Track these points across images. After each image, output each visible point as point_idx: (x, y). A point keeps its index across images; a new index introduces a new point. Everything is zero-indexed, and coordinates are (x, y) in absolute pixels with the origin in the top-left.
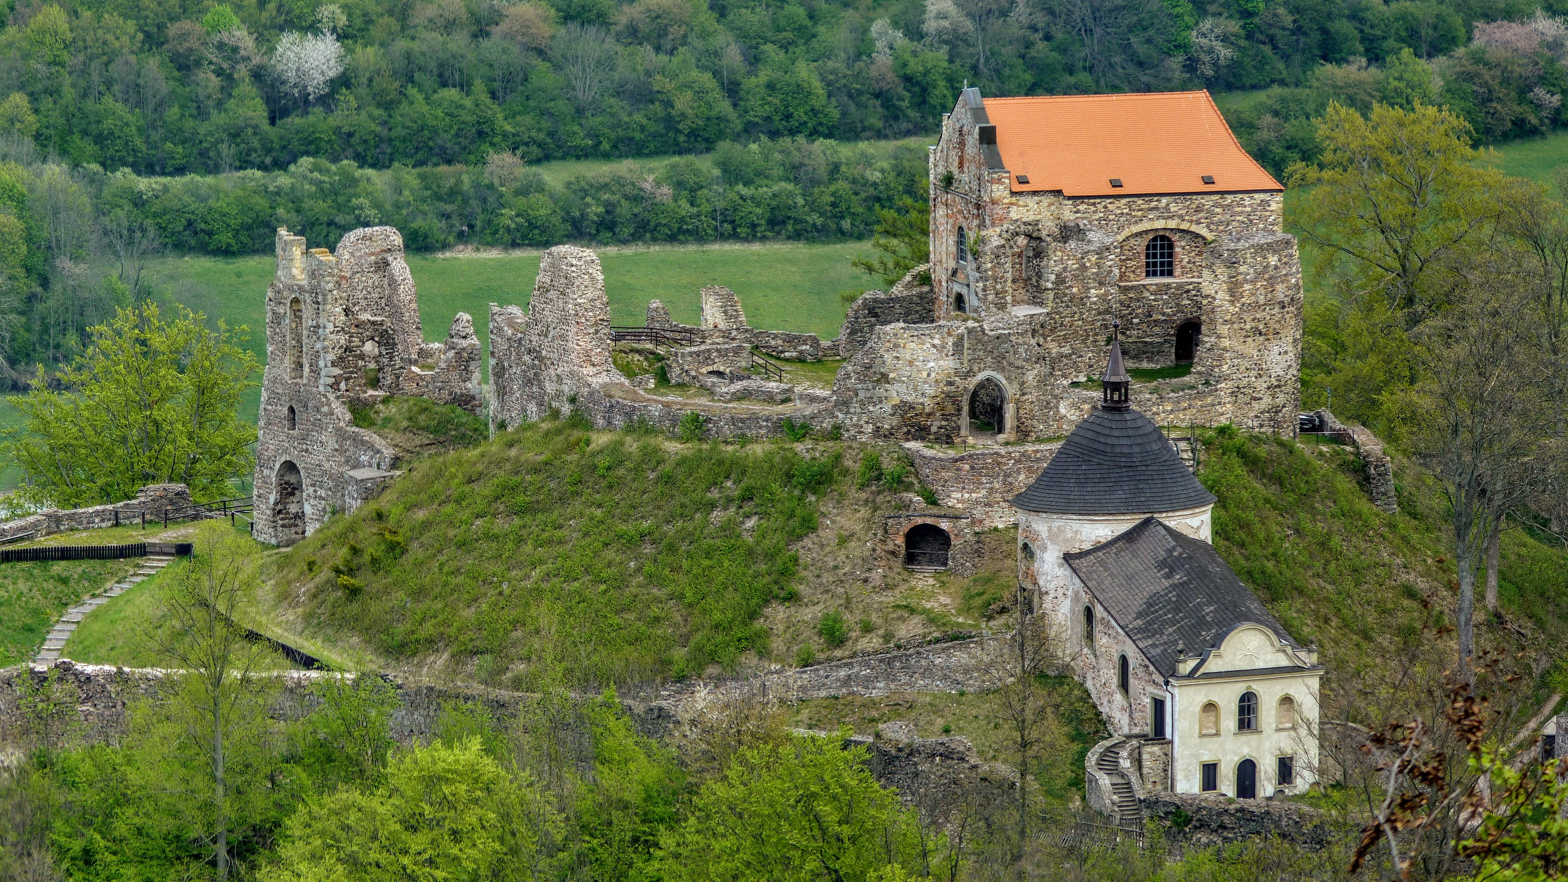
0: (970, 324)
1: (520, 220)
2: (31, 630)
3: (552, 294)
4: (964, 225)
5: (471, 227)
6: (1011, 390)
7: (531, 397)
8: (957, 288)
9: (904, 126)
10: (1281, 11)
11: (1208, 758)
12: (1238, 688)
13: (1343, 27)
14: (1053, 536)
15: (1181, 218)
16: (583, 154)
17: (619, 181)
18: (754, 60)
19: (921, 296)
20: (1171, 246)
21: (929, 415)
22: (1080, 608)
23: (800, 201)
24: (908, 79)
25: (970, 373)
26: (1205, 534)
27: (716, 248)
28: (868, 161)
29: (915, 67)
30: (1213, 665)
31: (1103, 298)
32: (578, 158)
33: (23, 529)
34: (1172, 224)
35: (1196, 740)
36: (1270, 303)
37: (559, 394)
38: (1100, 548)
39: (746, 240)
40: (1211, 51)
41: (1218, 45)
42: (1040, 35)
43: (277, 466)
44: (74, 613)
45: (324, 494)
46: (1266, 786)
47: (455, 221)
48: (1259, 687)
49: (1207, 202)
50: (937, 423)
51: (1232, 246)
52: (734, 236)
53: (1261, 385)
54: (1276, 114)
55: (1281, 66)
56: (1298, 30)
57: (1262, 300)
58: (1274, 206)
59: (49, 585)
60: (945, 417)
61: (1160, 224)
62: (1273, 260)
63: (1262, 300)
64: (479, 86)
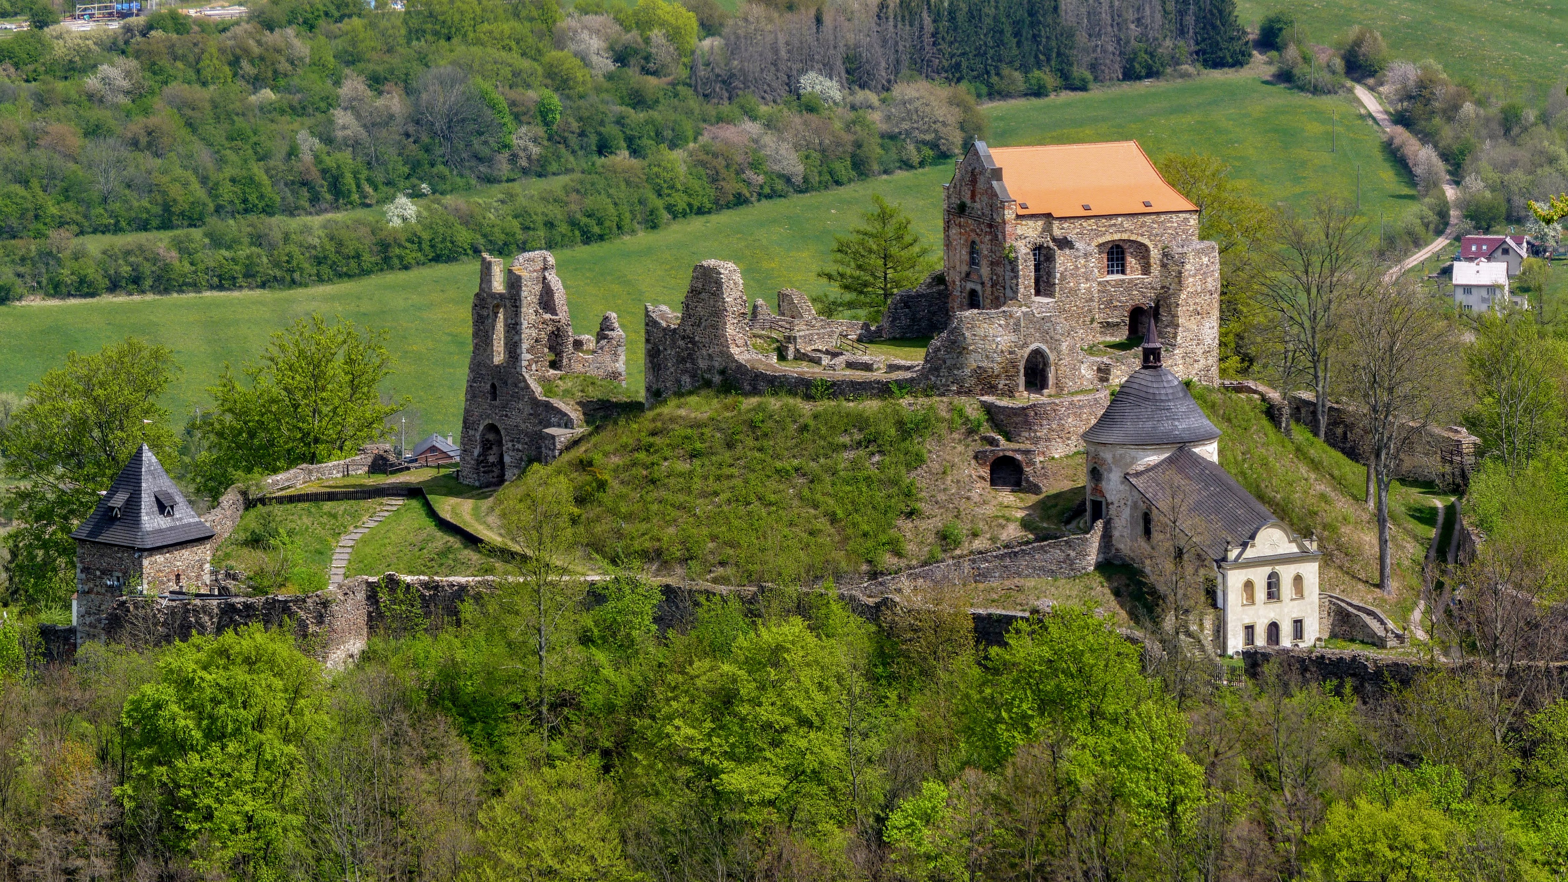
0: (1024, 309)
1: (74, 277)
2: (321, 553)
3: (704, 295)
4: (977, 239)
5: (39, 283)
6: (1052, 357)
7: (685, 371)
8: (970, 286)
9: (325, 206)
10: (571, 120)
11: (1248, 621)
12: (1268, 570)
13: (609, 129)
14: (1116, 461)
15: (1131, 231)
16: (104, 230)
17: (141, 249)
18: (221, 161)
19: (940, 293)
20: (1123, 253)
21: (998, 376)
22: (1139, 514)
23: (265, 260)
24: (324, 172)
25: (1025, 345)
26: (1215, 458)
27: (208, 294)
28: (307, 230)
29: (329, 162)
30: (1250, 553)
31: (1089, 290)
32: (103, 233)
33: (288, 480)
34: (1125, 236)
35: (1240, 608)
36: (1204, 291)
37: (710, 369)
38: (1149, 469)
39: (228, 289)
40: (525, 149)
41: (531, 145)
42: (411, 140)
43: (481, 428)
44: (346, 540)
45: (520, 447)
46: (1286, 641)
47: (28, 279)
48: (1278, 568)
49: (1149, 219)
50: (1003, 382)
51: (1180, 250)
52: (220, 287)
53: (1199, 351)
54: (578, 191)
55: (572, 159)
56: (582, 134)
57: (1199, 289)
58: (1192, 222)
59: (325, 520)
60: (1009, 378)
61: (1117, 237)
62: (1205, 260)
63: (1199, 289)
64: (35, 184)
